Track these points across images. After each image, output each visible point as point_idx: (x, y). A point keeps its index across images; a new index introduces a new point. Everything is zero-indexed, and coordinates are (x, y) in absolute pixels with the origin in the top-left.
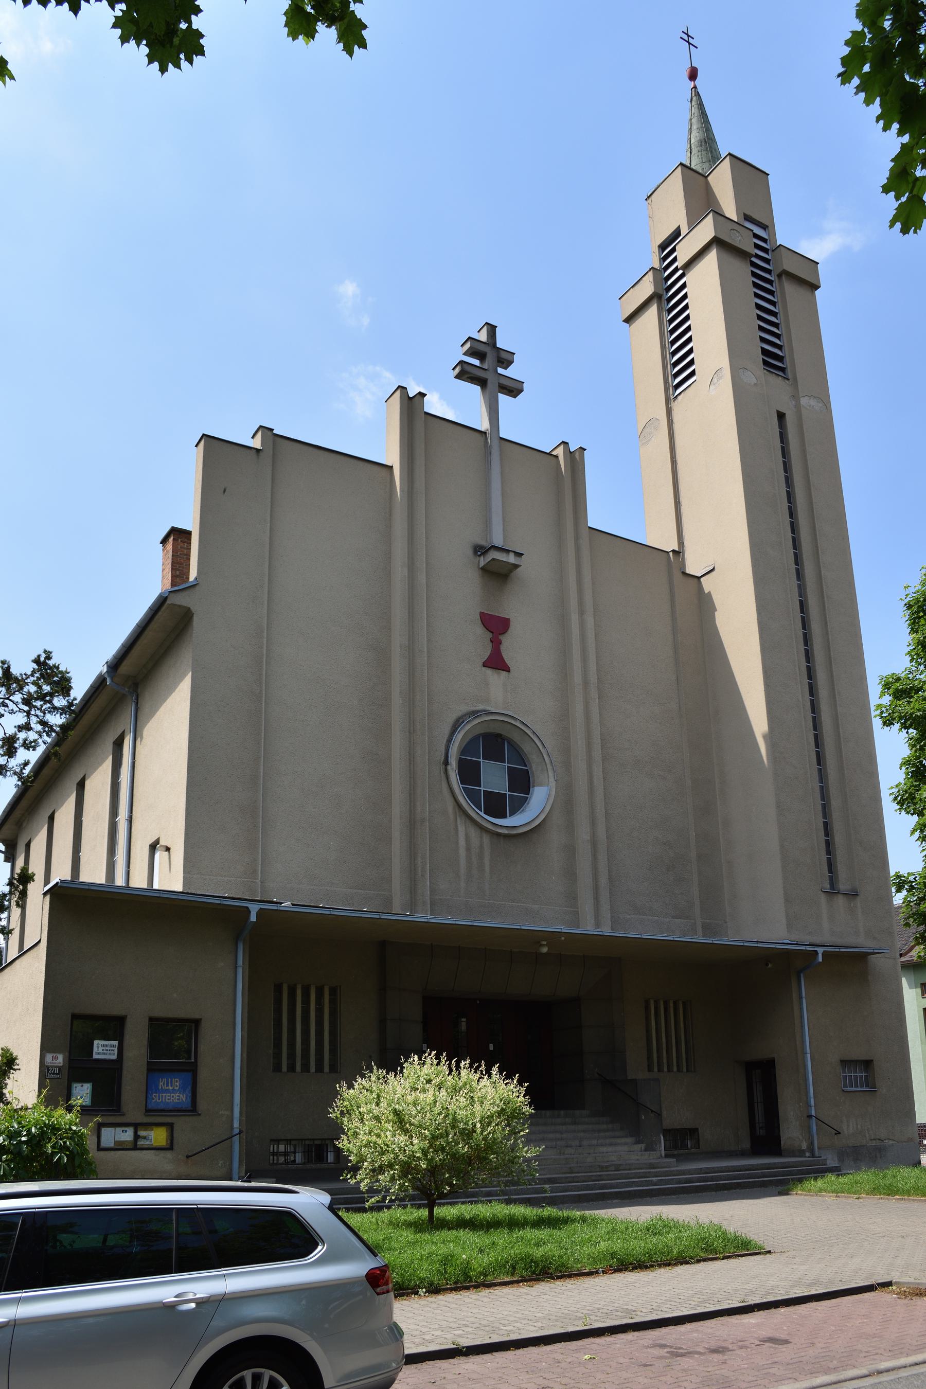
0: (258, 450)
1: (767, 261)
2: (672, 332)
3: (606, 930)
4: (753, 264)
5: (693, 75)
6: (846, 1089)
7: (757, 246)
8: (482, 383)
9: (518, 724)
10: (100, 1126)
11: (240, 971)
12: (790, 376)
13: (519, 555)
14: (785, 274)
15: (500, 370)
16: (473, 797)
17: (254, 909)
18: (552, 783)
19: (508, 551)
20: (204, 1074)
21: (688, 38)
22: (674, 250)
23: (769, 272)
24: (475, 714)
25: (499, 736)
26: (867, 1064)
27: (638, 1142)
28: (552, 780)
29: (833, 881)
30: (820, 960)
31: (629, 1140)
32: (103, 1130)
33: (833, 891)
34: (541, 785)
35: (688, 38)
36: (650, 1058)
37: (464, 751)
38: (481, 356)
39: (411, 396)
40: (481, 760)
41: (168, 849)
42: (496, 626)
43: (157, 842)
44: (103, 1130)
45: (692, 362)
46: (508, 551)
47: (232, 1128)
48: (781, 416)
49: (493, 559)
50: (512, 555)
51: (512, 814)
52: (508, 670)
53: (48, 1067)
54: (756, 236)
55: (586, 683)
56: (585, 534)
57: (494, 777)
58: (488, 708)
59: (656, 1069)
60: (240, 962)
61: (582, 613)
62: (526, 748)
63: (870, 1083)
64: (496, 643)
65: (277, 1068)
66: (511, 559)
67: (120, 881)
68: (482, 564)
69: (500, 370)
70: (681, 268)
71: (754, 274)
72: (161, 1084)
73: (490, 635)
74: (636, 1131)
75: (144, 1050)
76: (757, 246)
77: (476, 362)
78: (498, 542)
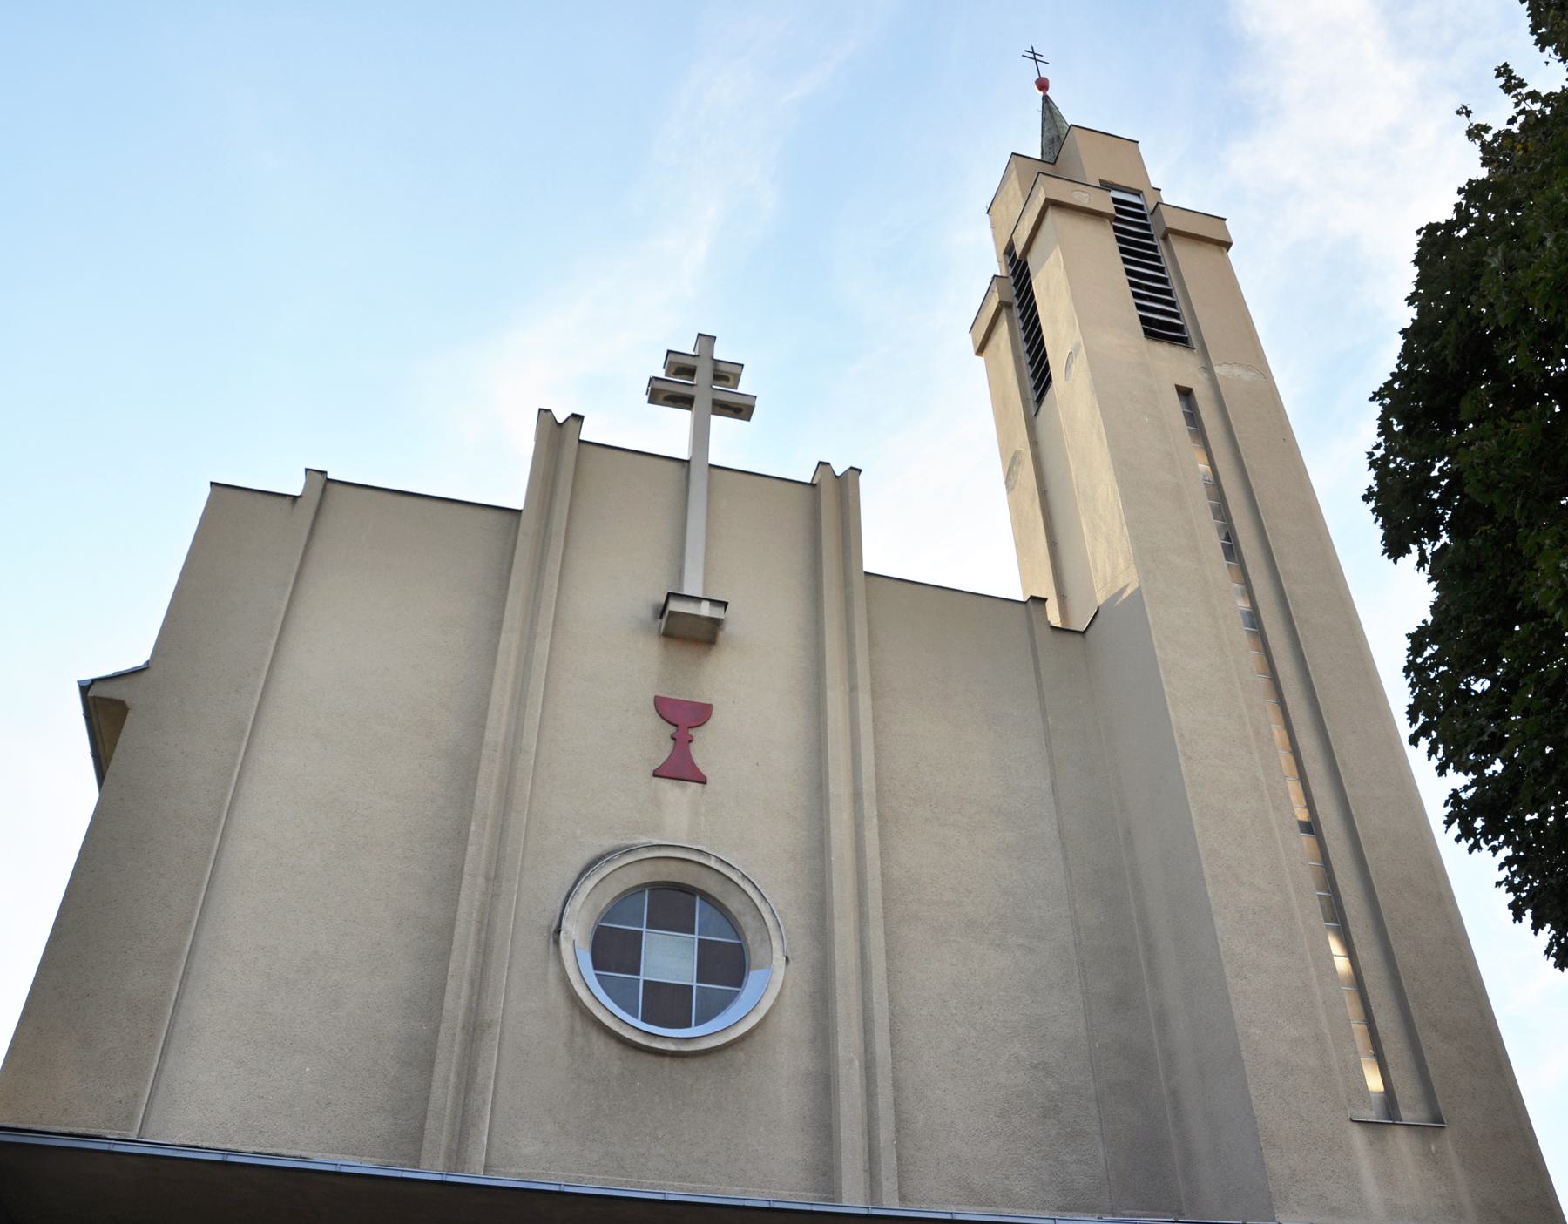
0: (295, 498)
5: (1042, 85)
9: (712, 863)
14: (1169, 233)
21: (1034, 56)
25: (689, 891)
34: (760, 967)
35: (1034, 56)
39: (560, 420)
40: (644, 929)
42: (683, 718)
46: (699, 599)
48: (1185, 393)
50: (706, 605)
52: (702, 781)
55: (857, 796)
56: (858, 583)
62: (734, 904)
64: (681, 742)
66: (705, 610)
73: (672, 729)
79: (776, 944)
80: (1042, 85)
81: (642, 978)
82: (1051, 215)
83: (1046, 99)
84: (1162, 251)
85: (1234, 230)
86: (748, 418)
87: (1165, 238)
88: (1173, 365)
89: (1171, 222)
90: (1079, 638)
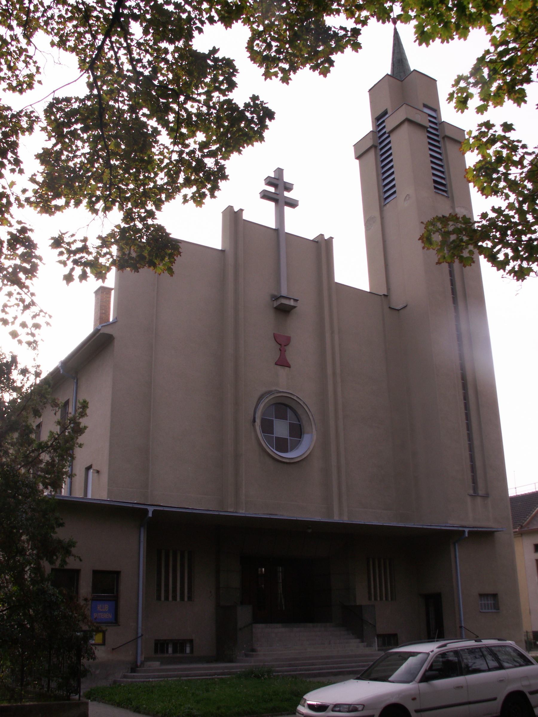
1: (436, 130)
2: (383, 167)
3: (345, 519)
6: (482, 611)
7: (430, 121)
8: (276, 201)
9: (295, 398)
11: (142, 544)
12: (450, 195)
14: (446, 137)
15: (286, 194)
16: (269, 440)
17: (151, 509)
18: (314, 432)
19: (290, 299)
20: (122, 602)
22: (383, 122)
24: (270, 393)
27: (363, 642)
28: (314, 430)
29: (475, 489)
30: (467, 535)
31: (358, 640)
33: (475, 495)
36: (369, 592)
37: (263, 414)
38: (275, 186)
41: (98, 472)
42: (282, 342)
46: (290, 299)
47: (137, 633)
49: (282, 304)
50: (292, 301)
51: (291, 450)
55: (334, 374)
57: (281, 429)
58: (278, 389)
59: (373, 599)
61: (332, 333)
62: (300, 412)
63: (496, 607)
65: (159, 598)
66: (292, 303)
68: (275, 305)
70: (388, 133)
72: (99, 608)
73: (279, 346)
74: (360, 635)
75: (90, 589)
76: (430, 121)
78: (284, 293)
81: (274, 436)
82: (406, 126)
83: (395, 29)
86: (329, 243)
89: (448, 133)
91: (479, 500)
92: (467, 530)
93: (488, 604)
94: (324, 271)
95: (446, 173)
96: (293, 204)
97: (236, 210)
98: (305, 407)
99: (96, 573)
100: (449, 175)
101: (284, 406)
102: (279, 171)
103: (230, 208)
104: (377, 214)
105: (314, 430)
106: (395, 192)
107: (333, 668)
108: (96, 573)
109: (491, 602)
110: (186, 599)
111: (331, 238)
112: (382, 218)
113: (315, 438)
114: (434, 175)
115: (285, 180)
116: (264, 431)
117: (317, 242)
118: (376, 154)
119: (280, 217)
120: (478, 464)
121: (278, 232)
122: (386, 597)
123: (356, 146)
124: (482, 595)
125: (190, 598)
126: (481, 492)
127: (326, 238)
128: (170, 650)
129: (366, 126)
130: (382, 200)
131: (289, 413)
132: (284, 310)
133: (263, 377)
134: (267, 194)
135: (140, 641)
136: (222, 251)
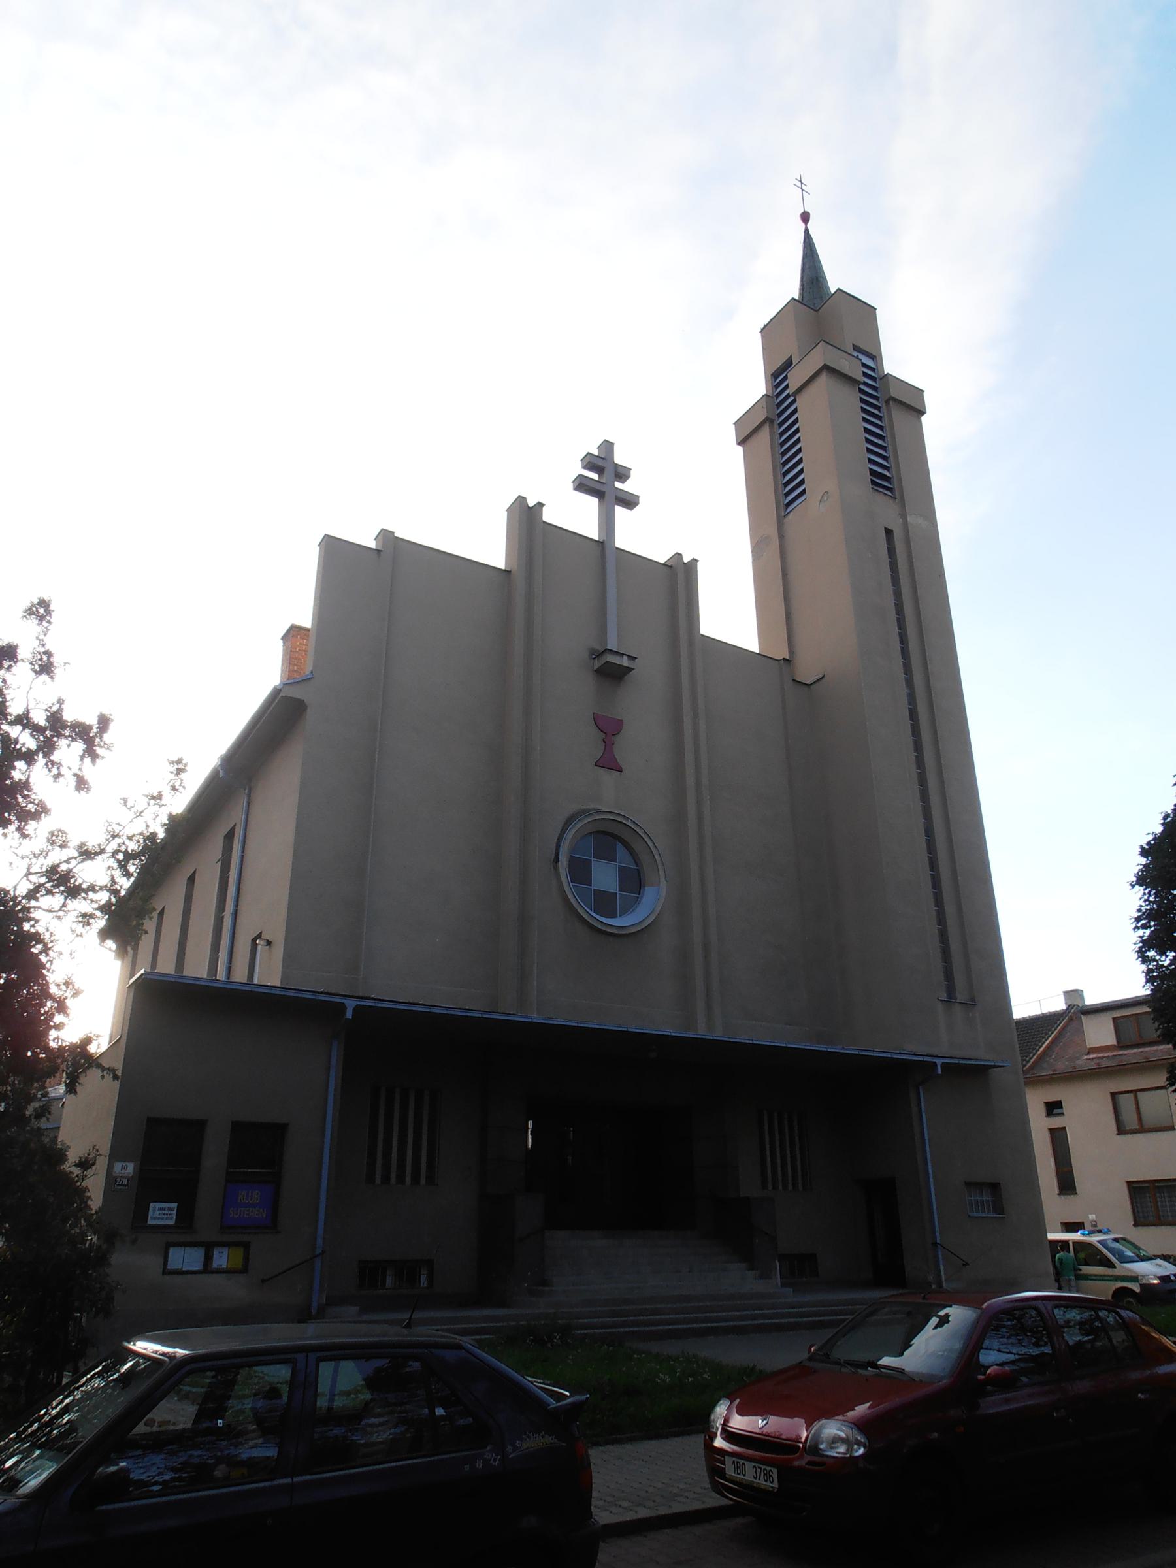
3: (719, 1035)
4: (861, 391)
5: (805, 217)
7: (865, 375)
10: (168, 1245)
11: (332, 1073)
13: (632, 658)
15: (618, 485)
17: (351, 1004)
18: (663, 884)
22: (786, 378)
23: (877, 398)
25: (615, 836)
26: (995, 1187)
28: (662, 879)
29: (951, 990)
32: (171, 1250)
42: (609, 729)
43: (259, 936)
44: (171, 1250)
45: (802, 482)
48: (889, 532)
50: (625, 658)
51: (624, 912)
53: (116, 1178)
54: (864, 365)
55: (698, 784)
57: (605, 877)
60: (334, 1062)
61: (695, 716)
62: (637, 847)
63: (998, 1207)
64: (608, 744)
65: (370, 1179)
66: (625, 662)
67: (221, 975)
69: (618, 485)
71: (862, 400)
76: (865, 375)
77: (595, 476)
78: (612, 644)
79: (661, 873)
80: (805, 217)
82: (824, 378)
83: (807, 231)
84: (883, 413)
85: (930, 402)
87: (887, 402)
88: (885, 511)
90: (806, 689)
91: (958, 1010)
92: (939, 1062)
93: (982, 1201)
94: (683, 623)
95: (892, 459)
96: (630, 502)
97: (531, 504)
98: (647, 839)
99: (238, 1128)
100: (897, 464)
101: (610, 837)
102: (608, 446)
103: (521, 500)
104: (773, 531)
105: (662, 879)
106: (804, 492)
107: (696, 1320)
108: (238, 1128)
109: (987, 1198)
110: (423, 1181)
111: (695, 561)
112: (782, 537)
113: (664, 893)
114: (870, 461)
115: (617, 461)
116: (574, 879)
117: (671, 567)
118: (772, 433)
119: (607, 523)
120: (955, 946)
121: (603, 547)
122: (794, 1185)
123: (738, 424)
124: (968, 1184)
125: (431, 1180)
126: (961, 996)
127: (686, 561)
128: (389, 1281)
129: (752, 386)
130: (782, 507)
131: (620, 850)
132: (611, 673)
133: (570, 782)
134: (585, 482)
135: (318, 1263)
136: (507, 572)
